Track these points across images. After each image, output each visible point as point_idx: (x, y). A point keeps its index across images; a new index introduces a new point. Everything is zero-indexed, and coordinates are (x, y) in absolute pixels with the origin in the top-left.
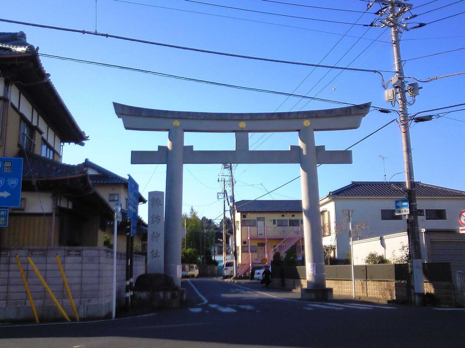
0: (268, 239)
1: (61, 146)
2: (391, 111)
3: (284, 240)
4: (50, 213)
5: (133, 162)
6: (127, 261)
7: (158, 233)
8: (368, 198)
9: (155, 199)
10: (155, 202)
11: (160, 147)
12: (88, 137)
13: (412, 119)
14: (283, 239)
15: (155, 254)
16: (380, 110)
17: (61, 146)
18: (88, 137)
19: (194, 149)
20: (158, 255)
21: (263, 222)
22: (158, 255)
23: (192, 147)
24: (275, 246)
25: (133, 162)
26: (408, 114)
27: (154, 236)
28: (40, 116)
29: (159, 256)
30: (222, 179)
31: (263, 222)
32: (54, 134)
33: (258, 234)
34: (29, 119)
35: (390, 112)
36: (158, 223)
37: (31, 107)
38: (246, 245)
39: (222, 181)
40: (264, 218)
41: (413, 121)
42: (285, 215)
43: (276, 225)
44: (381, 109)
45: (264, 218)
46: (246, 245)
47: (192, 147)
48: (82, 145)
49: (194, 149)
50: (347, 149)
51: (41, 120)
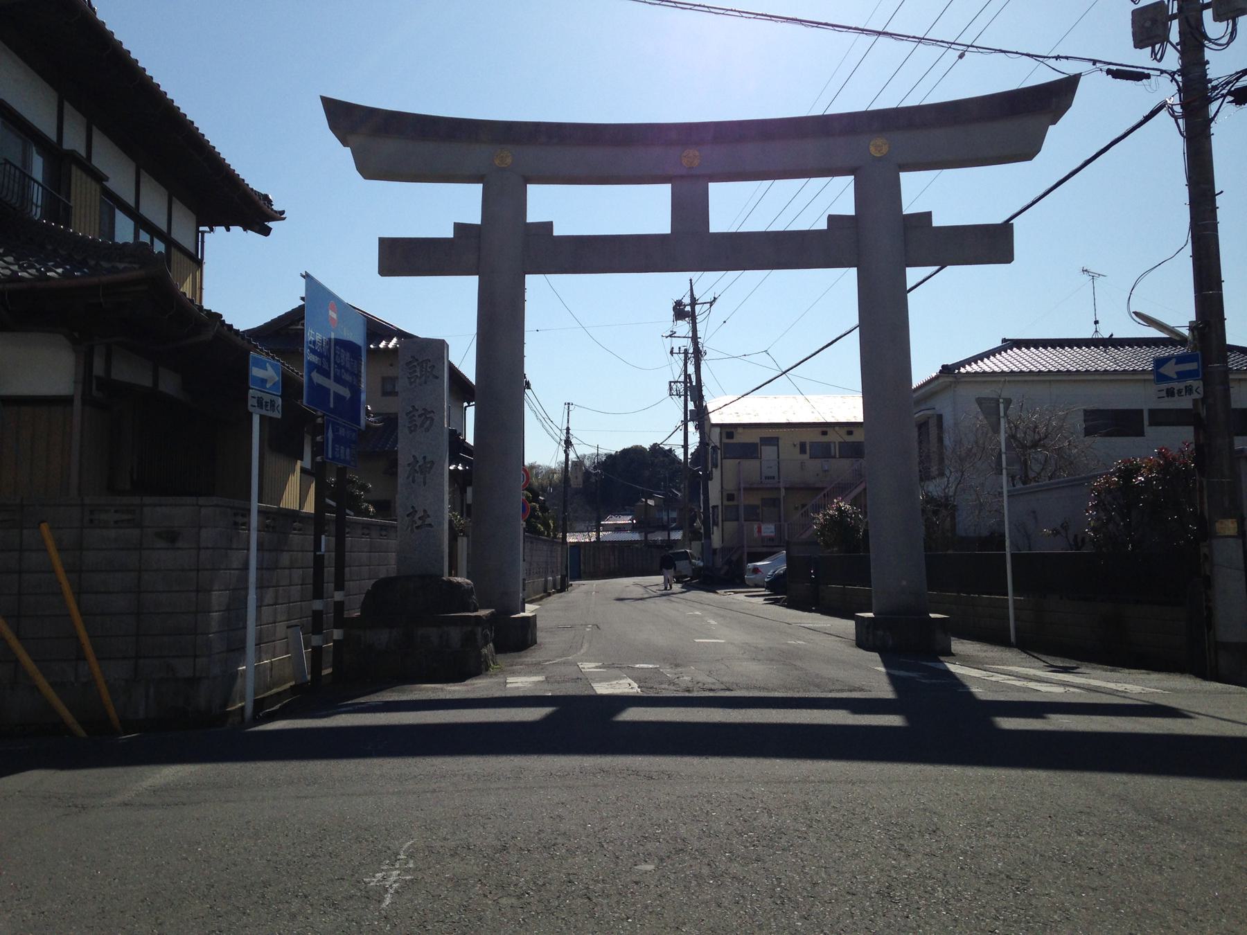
0: (786, 489)
1: (200, 234)
2: (1151, 72)
3: (825, 492)
4: (67, 396)
5: (387, 268)
6: (1243, 542)
7: (427, 460)
8: (1048, 380)
9: (417, 360)
10: (418, 370)
11: (458, 227)
12: (283, 212)
13: (1224, 96)
14: (823, 489)
15: (419, 518)
16: (1109, 72)
17: (200, 234)
18: (283, 212)
19: (556, 233)
20: (428, 521)
21: (775, 448)
22: (428, 521)
23: (549, 225)
24: (803, 506)
25: (387, 268)
26: (1210, 81)
27: (417, 468)
28: (94, 128)
29: (430, 525)
30: (680, 348)
31: (775, 448)
32: (166, 198)
33: (763, 478)
34: (50, 131)
35: (1148, 76)
36: (427, 430)
37: (52, 97)
38: (735, 503)
39: (680, 353)
40: (777, 439)
41: (1227, 100)
42: (829, 433)
43: (806, 456)
44: (1114, 68)
45: (777, 439)
46: (735, 503)
47: (549, 225)
48: (266, 232)
49: (556, 233)
50: (969, 361)
51: (99, 140)
